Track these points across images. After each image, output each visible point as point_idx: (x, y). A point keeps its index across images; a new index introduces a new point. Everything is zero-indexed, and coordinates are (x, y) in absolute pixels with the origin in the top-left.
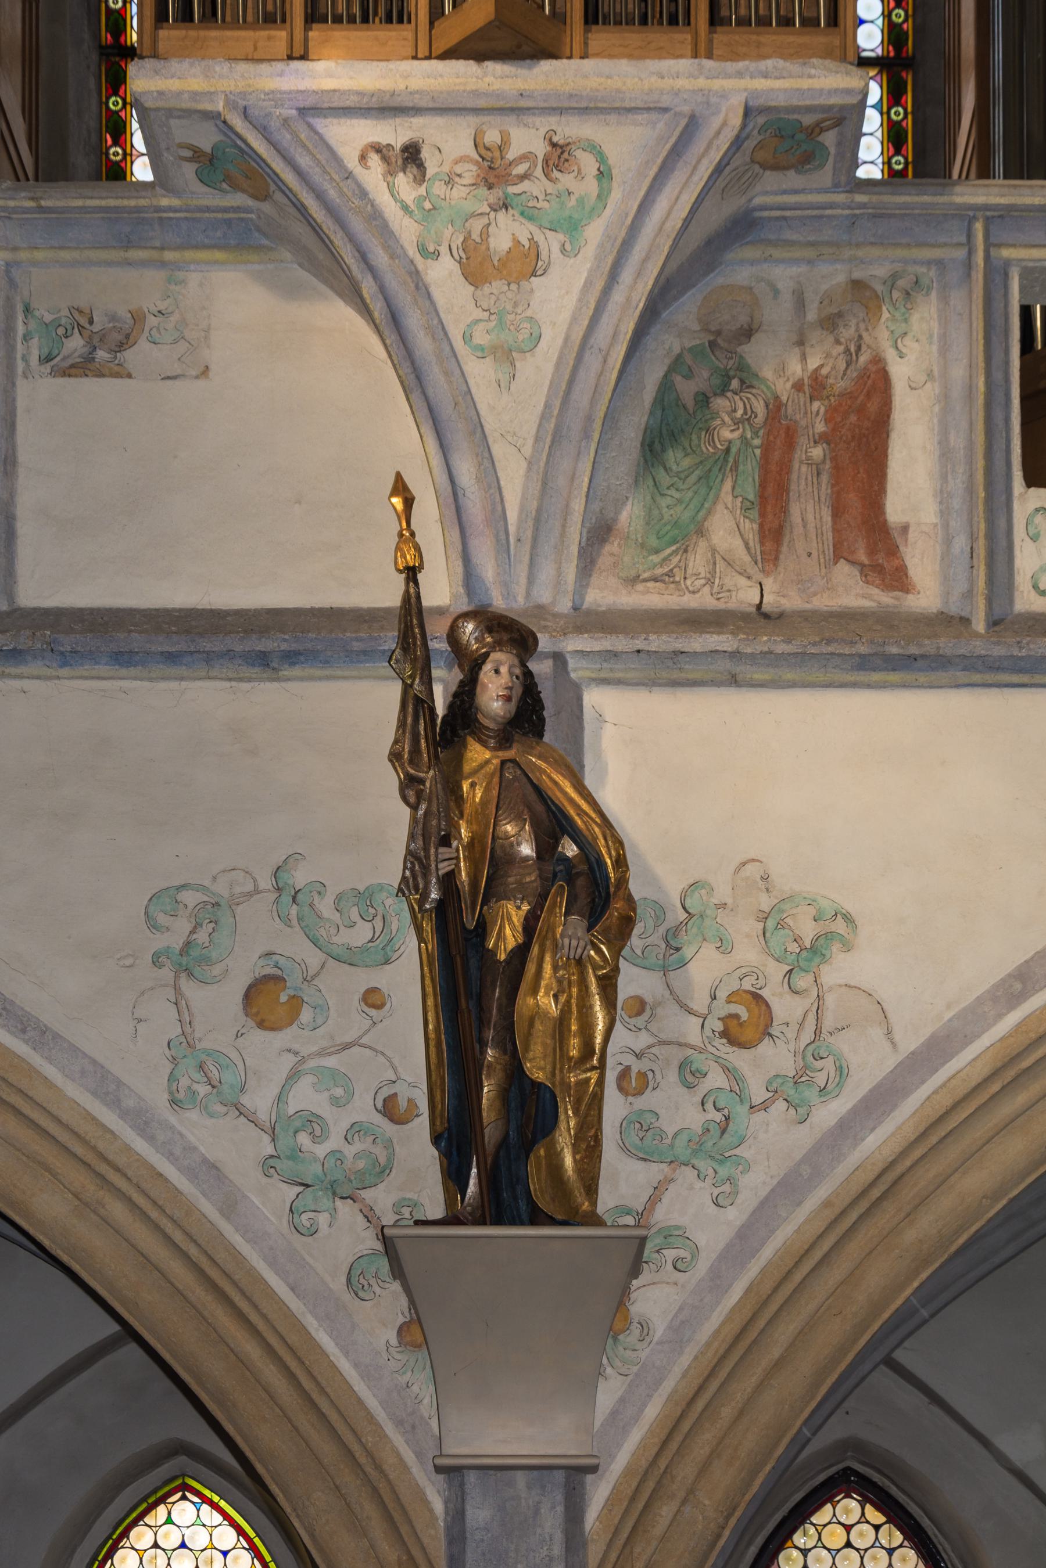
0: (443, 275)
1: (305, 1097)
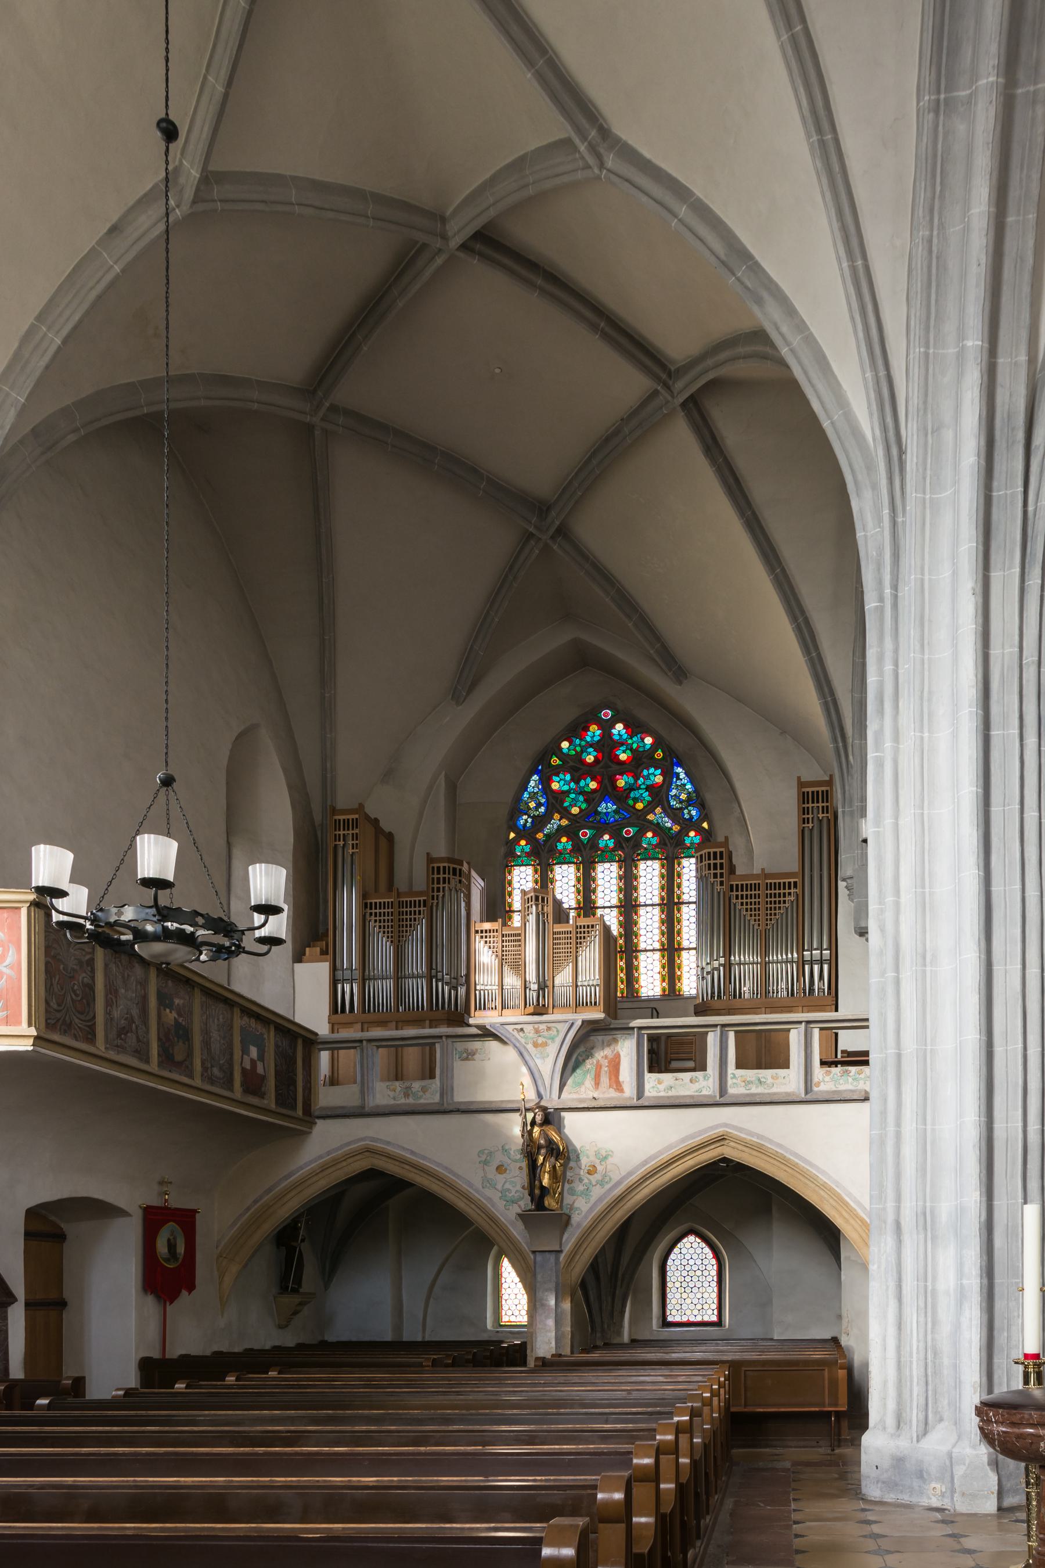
0: (530, 1047)
1: (507, 1186)
